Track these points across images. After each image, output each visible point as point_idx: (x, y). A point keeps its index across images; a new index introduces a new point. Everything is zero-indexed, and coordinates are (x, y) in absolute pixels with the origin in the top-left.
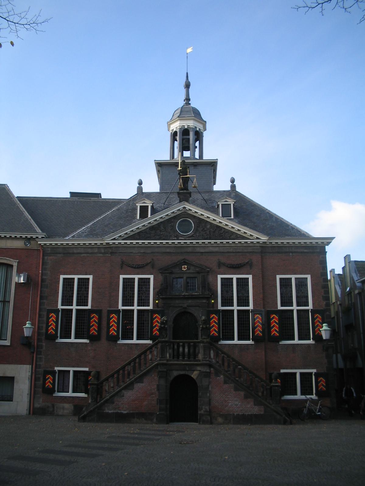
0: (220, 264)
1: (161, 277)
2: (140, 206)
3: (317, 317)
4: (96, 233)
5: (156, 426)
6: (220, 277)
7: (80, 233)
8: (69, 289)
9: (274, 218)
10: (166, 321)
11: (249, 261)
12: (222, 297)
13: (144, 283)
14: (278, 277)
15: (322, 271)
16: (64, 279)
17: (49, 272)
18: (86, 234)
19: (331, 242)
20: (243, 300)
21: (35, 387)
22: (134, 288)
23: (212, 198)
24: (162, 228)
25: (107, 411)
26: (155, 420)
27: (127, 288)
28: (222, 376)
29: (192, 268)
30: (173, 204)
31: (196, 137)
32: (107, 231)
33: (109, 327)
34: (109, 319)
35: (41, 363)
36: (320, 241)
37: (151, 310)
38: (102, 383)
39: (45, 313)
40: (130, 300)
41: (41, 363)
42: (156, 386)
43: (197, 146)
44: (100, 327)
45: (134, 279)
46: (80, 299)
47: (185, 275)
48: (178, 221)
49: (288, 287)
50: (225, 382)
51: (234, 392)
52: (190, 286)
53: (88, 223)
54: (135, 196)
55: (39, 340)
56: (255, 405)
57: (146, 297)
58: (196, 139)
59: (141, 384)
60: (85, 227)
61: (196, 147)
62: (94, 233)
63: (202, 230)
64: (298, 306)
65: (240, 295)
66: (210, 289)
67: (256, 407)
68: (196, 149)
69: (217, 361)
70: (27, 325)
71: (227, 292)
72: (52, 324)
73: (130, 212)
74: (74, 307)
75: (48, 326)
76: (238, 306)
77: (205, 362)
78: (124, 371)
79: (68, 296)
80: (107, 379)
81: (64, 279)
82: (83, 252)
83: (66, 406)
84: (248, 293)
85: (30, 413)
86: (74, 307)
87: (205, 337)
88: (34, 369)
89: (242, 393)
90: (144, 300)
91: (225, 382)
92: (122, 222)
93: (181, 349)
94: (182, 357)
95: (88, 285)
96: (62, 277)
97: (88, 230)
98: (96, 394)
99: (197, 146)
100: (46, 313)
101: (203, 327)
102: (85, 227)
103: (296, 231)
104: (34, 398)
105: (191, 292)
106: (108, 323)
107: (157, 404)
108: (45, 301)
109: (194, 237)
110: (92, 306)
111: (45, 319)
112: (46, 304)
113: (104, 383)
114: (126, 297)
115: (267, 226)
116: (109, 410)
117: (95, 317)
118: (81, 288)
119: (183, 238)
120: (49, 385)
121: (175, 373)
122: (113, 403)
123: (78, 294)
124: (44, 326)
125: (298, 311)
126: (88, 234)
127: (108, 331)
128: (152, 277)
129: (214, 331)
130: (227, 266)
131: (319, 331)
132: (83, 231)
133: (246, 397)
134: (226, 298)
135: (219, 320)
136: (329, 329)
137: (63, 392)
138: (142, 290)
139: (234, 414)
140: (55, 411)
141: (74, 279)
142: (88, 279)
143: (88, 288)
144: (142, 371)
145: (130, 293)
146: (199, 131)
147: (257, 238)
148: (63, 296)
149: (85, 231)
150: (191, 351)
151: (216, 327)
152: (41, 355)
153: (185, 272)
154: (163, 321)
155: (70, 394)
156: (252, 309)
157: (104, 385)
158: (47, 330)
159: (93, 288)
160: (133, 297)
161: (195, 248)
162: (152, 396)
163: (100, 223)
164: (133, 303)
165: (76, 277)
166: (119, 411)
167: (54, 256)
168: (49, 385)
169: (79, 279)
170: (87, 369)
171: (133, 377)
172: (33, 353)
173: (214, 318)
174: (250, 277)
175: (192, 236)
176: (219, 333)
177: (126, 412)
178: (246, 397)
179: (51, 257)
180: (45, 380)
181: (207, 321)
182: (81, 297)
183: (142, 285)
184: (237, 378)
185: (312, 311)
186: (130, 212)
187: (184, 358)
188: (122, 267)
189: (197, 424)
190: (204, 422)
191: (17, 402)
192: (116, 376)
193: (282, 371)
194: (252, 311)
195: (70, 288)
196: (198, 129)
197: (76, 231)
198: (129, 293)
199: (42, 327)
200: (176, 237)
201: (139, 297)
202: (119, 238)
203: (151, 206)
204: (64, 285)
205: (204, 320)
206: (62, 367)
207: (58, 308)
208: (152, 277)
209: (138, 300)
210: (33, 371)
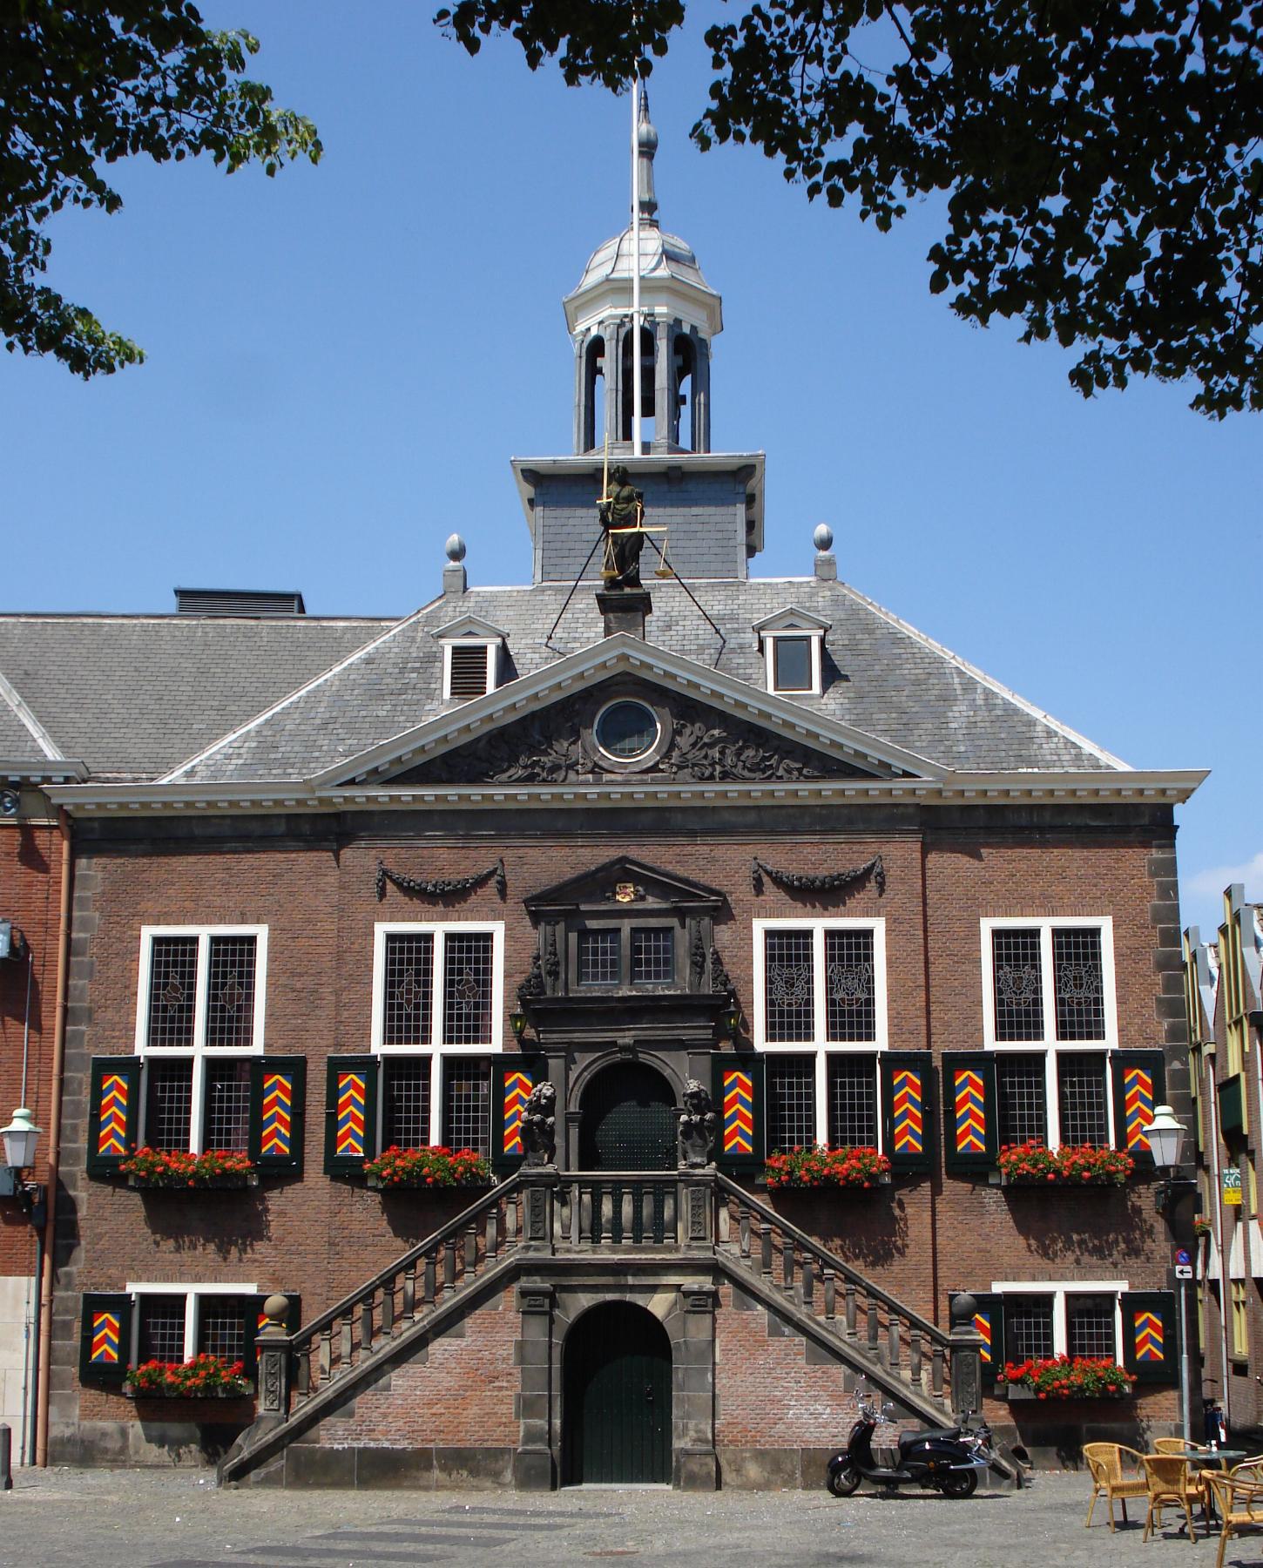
2: (454, 648)
4: (280, 755)
5: (513, 1498)
6: (760, 926)
7: (219, 757)
8: (177, 982)
9: (979, 691)
10: (551, 1100)
11: (874, 865)
14: (987, 925)
16: (158, 941)
17: (97, 914)
18: (241, 761)
19: (1193, 790)
20: (790, 1014)
23: (741, 611)
25: (328, 1446)
26: (508, 1476)
27: (225, 973)
30: (585, 635)
31: (680, 360)
32: (325, 748)
33: (332, 1123)
34: (333, 1093)
37: (495, 1055)
38: (307, 1340)
39: (84, 1077)
40: (417, 1019)
42: (509, 1350)
43: (684, 397)
46: (223, 1020)
47: (626, 921)
48: (598, 710)
49: (1024, 966)
51: (808, 1368)
53: (249, 716)
54: (437, 604)
57: (477, 1006)
58: (679, 368)
61: (683, 400)
62: (272, 756)
63: (694, 745)
64: (1062, 1036)
65: (837, 997)
66: (722, 978)
68: (682, 407)
69: (744, 1251)
70: (19, 1125)
71: (790, 983)
73: (414, 670)
75: (95, 1125)
76: (832, 1037)
78: (391, 1293)
79: (172, 1006)
80: (325, 1326)
81: (158, 941)
84: (868, 989)
86: (199, 1050)
87: (698, 1160)
88: (45, 1291)
90: (468, 1019)
92: (385, 713)
94: (631, 1235)
96: (148, 933)
97: (246, 745)
98: (283, 1381)
99: (684, 397)
103: (1061, 745)
104: (48, 1403)
107: (517, 1417)
108: (83, 1028)
109: (662, 771)
110: (267, 1045)
111: (85, 1098)
112: (86, 1038)
113: (317, 1338)
116: (334, 1436)
117: (277, 1088)
118: (225, 975)
120: (105, 1351)
122: (351, 1415)
123: (212, 997)
124: (84, 1123)
126: (249, 762)
127: (332, 1141)
128: (498, 929)
131: (1140, 1136)
132: (231, 751)
134: (786, 1008)
136: (1178, 1126)
138: (462, 980)
140: (131, 1451)
141: (194, 940)
143: (428, 972)
144: (460, 1291)
145: (417, 993)
146: (693, 338)
147: (907, 774)
149: (237, 751)
150: (647, 1210)
153: (625, 907)
157: (313, 1346)
161: (667, 814)
162: (496, 1384)
163: (296, 716)
164: (427, 1029)
165: (204, 933)
166: (372, 1445)
170: (250, 1289)
171: (423, 1317)
173: (739, 1086)
175: (654, 769)
181: (712, 1101)
182: (223, 1009)
184: (819, 1314)
186: (414, 670)
187: (617, 1238)
189: (670, 1487)
190: (692, 1482)
192: (359, 1310)
193: (998, 1288)
195: (477, 972)
196: (686, 329)
197: (202, 748)
198: (409, 992)
199: (75, 1128)
202: (370, 779)
203: (498, 647)
206: (156, 1281)
207: (136, 1054)
208: (498, 929)
210: (44, 1300)
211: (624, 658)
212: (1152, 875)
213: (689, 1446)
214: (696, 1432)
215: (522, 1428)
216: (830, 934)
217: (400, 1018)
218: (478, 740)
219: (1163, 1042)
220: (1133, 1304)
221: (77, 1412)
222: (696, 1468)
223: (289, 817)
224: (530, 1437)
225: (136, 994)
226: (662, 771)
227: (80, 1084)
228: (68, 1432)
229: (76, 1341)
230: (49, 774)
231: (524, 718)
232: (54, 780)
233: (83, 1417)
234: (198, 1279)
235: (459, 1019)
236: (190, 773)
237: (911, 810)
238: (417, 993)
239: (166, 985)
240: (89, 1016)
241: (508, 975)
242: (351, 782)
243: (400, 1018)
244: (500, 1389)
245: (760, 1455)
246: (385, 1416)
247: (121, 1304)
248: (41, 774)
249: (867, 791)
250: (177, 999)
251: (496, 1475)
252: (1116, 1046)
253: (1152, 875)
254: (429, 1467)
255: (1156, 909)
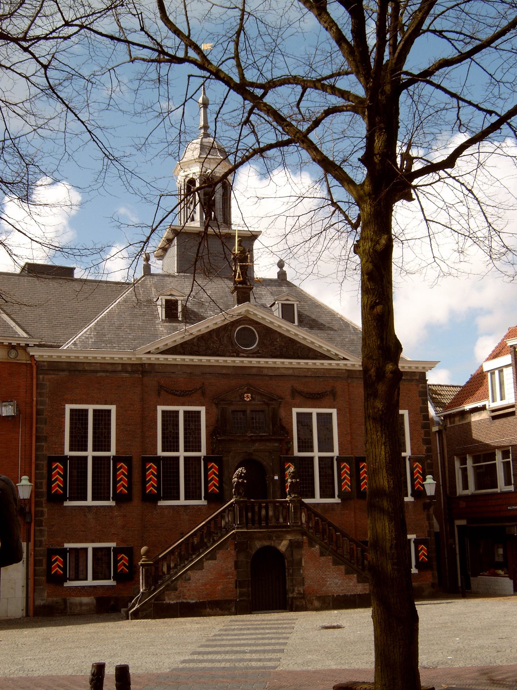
0: (294, 393)
1: (215, 410)
3: (121, 467)
8: (80, 426)
12: (299, 438)
13: (324, 420)
15: (421, 405)
21: (35, 575)
22: (177, 425)
24: (216, 338)
25: (168, 602)
28: (317, 547)
29: (258, 397)
33: (144, 482)
35: (43, 539)
36: (420, 366)
39: (45, 463)
41: (43, 539)
44: (130, 483)
45: (177, 412)
50: (322, 554)
52: (256, 423)
55: (38, 504)
56: (359, 582)
59: (214, 562)
60: (86, 329)
66: (283, 428)
67: (360, 584)
72: (151, 479)
74: (90, 453)
75: (50, 483)
77: (295, 528)
79: (78, 436)
82: (99, 369)
83: (85, 600)
85: (27, 615)
89: (343, 568)
91: (322, 554)
93: (263, 512)
95: (109, 420)
96: (68, 407)
100: (46, 462)
101: (292, 482)
102: (86, 329)
105: (257, 432)
106: (144, 476)
107: (236, 588)
108: (43, 444)
109: (260, 353)
111: (45, 471)
112: (44, 448)
114: (167, 438)
115: (346, 340)
116: (170, 600)
119: (245, 355)
120: (56, 569)
121: (258, 545)
122: (176, 589)
124: (45, 481)
125: (186, 458)
127: (144, 488)
128: (203, 410)
129: (151, 488)
130: (305, 397)
133: (347, 572)
135: (158, 470)
137: (77, 579)
139: (333, 596)
140: (68, 609)
142: (109, 411)
143: (109, 424)
147: (344, 359)
148: (71, 437)
151: (60, 481)
152: (42, 526)
154: (241, 473)
155: (90, 582)
156: (205, 455)
158: (49, 488)
159: (339, 425)
160: (86, 437)
166: (184, 601)
167: (54, 374)
168: (56, 569)
169: (95, 411)
172: (30, 523)
174: (334, 411)
175: (257, 352)
176: (64, 489)
177: (193, 601)
178: (347, 572)
179: (50, 377)
180: (50, 563)
183: (189, 422)
185: (338, 459)
188: (159, 394)
191: (8, 599)
194: (116, 459)
200: (235, 352)
201: (185, 438)
204: (71, 419)
205: (293, 472)
209: (185, 442)
211: (247, 311)
212: (420, 396)
213: (295, 596)
214: (298, 591)
215: (238, 592)
216: (185, 412)
217: (167, 442)
218: (194, 338)
219: (424, 453)
220: (117, 551)
221: (46, 594)
222: (298, 603)
223: (122, 364)
224: (241, 595)
225: (64, 431)
226: (260, 353)
227: (43, 466)
228: (42, 603)
229: (44, 567)
230: (28, 343)
231: (211, 331)
232: (30, 345)
233: (48, 596)
234: (93, 541)
235: (189, 443)
236: (75, 344)
237: (344, 371)
238: (173, 433)
239: (76, 428)
240: (45, 439)
241: (207, 427)
242: (149, 353)
243: (167, 442)
244: (230, 578)
245: (319, 598)
246: (189, 590)
247: (63, 552)
248: (26, 343)
249: (105, 358)
250: (81, 433)
251: (229, 609)
252: (114, 454)
253: (420, 396)
254: (205, 608)
255: (421, 408)
